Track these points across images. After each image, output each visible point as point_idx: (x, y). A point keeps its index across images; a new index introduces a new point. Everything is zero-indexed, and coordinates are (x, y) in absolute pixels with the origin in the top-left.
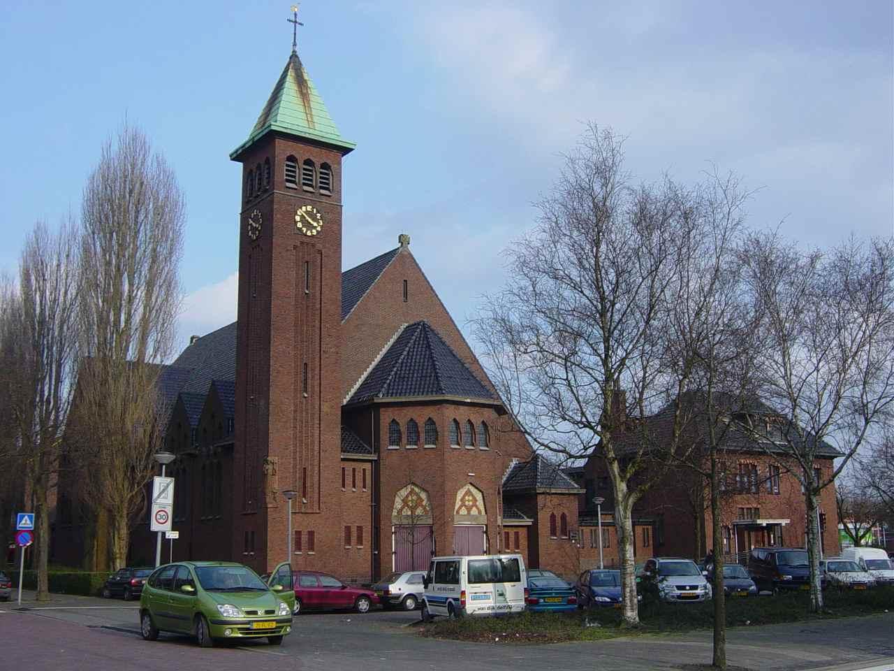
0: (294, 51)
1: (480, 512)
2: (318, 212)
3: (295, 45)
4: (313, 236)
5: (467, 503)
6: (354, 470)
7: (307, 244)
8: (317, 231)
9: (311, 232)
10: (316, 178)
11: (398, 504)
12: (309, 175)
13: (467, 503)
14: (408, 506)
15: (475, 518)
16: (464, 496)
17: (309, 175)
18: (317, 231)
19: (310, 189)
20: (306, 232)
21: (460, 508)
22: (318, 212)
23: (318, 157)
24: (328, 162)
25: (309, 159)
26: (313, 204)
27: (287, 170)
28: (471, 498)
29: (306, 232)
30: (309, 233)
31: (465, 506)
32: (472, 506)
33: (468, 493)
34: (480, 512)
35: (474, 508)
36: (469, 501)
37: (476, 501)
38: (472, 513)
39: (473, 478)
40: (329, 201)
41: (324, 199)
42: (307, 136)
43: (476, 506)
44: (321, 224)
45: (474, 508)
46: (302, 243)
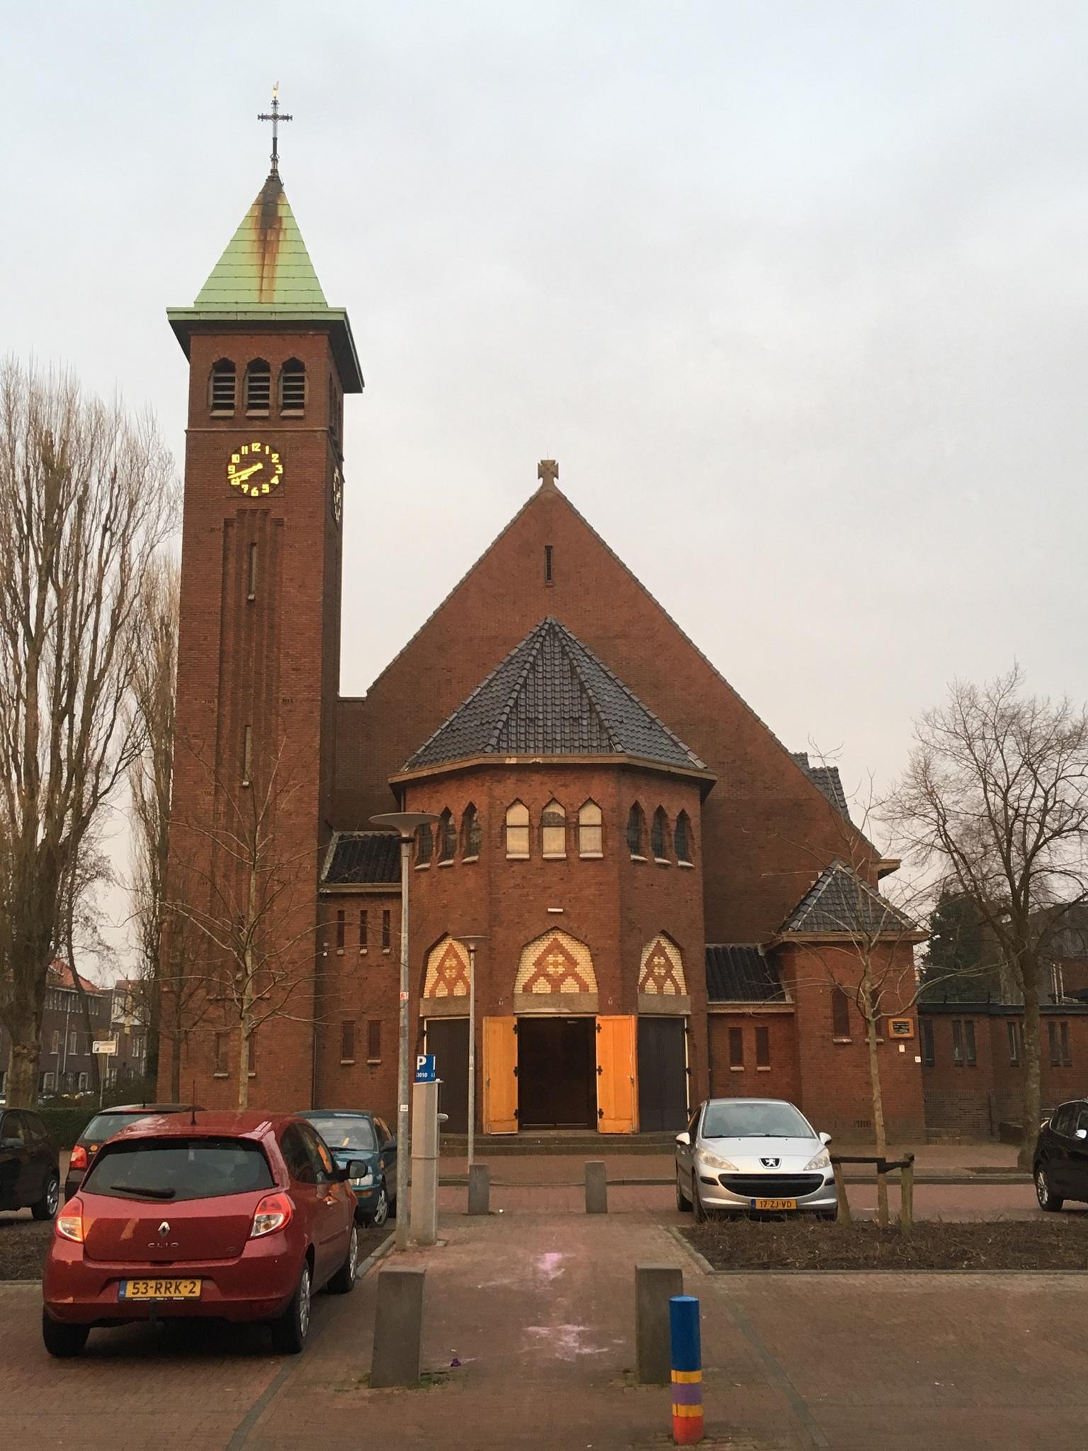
0: (274, 171)
1: (678, 990)
2: (273, 450)
3: (275, 160)
4: (262, 496)
5: (656, 970)
6: (364, 913)
7: (254, 512)
8: (271, 485)
9: (260, 490)
10: (275, 391)
11: (527, 969)
12: (261, 388)
13: (551, 970)
14: (547, 976)
15: (569, 999)
16: (443, 960)
17: (261, 388)
18: (271, 485)
19: (264, 413)
20: (250, 490)
21: (646, 979)
22: (273, 450)
23: (276, 353)
24: (301, 357)
25: (293, 359)
26: (264, 438)
27: (267, 397)
28: (662, 961)
29: (250, 490)
30: (255, 492)
31: (547, 976)
32: (456, 980)
33: (451, 952)
34: (678, 990)
35: (669, 982)
36: (556, 964)
37: (575, 964)
38: (564, 989)
39: (562, 918)
40: (301, 427)
41: (289, 426)
42: (240, 317)
43: (577, 977)
44: (281, 471)
45: (460, 984)
46: (242, 512)
